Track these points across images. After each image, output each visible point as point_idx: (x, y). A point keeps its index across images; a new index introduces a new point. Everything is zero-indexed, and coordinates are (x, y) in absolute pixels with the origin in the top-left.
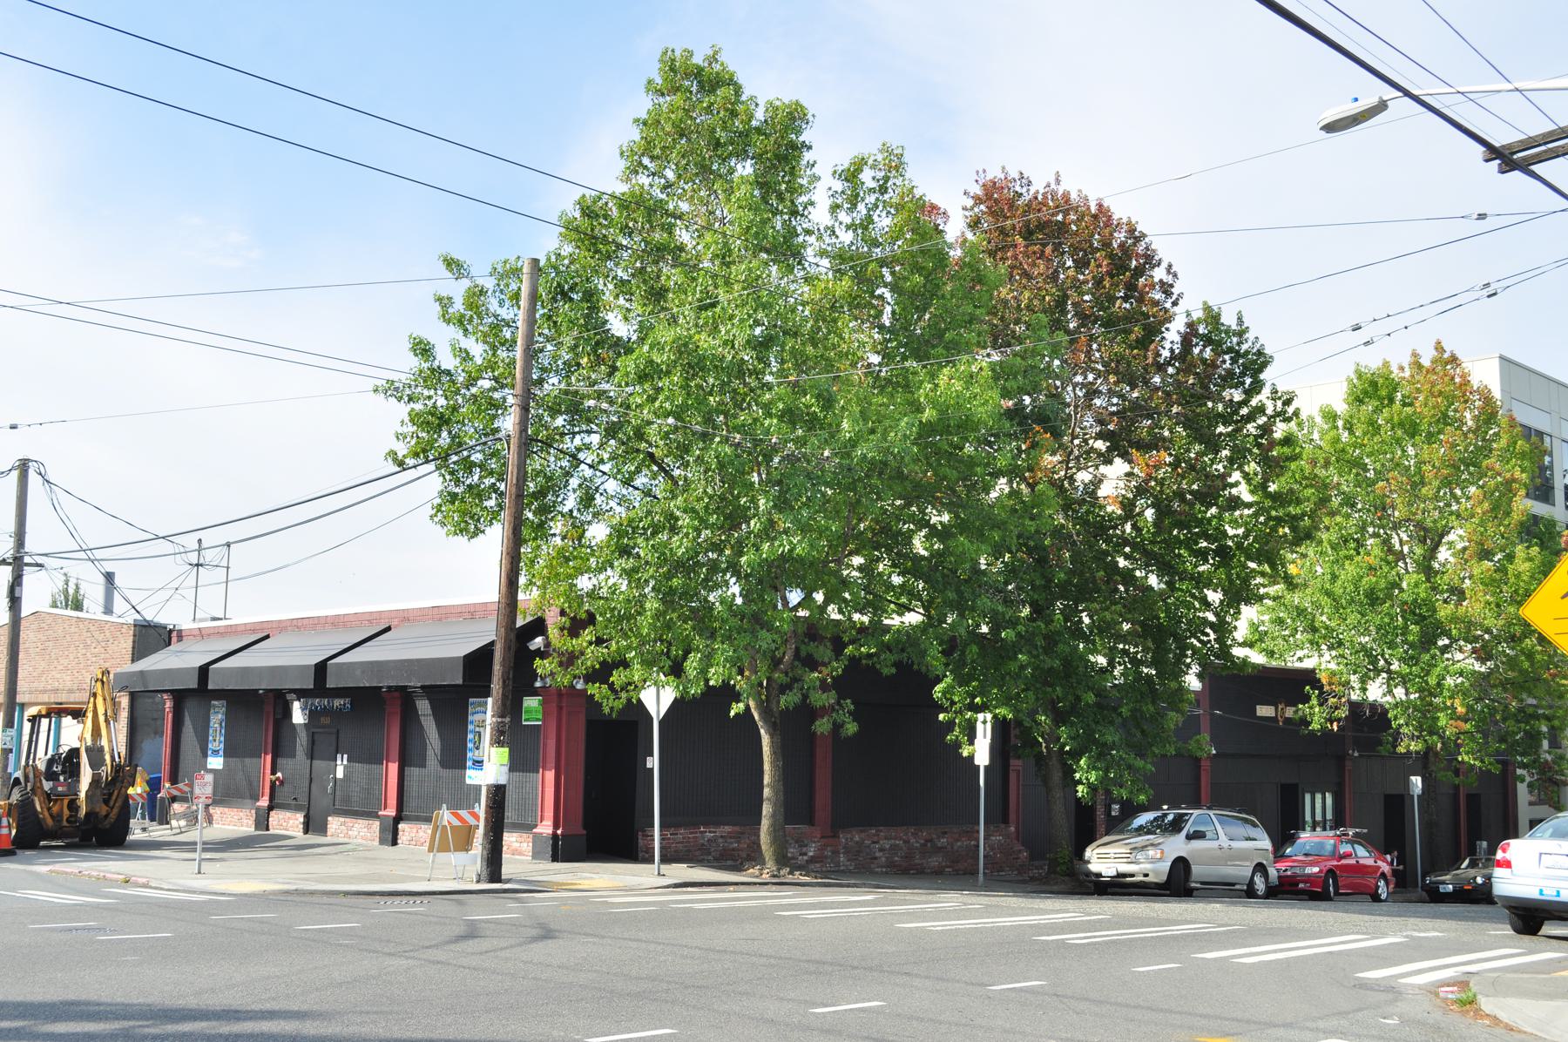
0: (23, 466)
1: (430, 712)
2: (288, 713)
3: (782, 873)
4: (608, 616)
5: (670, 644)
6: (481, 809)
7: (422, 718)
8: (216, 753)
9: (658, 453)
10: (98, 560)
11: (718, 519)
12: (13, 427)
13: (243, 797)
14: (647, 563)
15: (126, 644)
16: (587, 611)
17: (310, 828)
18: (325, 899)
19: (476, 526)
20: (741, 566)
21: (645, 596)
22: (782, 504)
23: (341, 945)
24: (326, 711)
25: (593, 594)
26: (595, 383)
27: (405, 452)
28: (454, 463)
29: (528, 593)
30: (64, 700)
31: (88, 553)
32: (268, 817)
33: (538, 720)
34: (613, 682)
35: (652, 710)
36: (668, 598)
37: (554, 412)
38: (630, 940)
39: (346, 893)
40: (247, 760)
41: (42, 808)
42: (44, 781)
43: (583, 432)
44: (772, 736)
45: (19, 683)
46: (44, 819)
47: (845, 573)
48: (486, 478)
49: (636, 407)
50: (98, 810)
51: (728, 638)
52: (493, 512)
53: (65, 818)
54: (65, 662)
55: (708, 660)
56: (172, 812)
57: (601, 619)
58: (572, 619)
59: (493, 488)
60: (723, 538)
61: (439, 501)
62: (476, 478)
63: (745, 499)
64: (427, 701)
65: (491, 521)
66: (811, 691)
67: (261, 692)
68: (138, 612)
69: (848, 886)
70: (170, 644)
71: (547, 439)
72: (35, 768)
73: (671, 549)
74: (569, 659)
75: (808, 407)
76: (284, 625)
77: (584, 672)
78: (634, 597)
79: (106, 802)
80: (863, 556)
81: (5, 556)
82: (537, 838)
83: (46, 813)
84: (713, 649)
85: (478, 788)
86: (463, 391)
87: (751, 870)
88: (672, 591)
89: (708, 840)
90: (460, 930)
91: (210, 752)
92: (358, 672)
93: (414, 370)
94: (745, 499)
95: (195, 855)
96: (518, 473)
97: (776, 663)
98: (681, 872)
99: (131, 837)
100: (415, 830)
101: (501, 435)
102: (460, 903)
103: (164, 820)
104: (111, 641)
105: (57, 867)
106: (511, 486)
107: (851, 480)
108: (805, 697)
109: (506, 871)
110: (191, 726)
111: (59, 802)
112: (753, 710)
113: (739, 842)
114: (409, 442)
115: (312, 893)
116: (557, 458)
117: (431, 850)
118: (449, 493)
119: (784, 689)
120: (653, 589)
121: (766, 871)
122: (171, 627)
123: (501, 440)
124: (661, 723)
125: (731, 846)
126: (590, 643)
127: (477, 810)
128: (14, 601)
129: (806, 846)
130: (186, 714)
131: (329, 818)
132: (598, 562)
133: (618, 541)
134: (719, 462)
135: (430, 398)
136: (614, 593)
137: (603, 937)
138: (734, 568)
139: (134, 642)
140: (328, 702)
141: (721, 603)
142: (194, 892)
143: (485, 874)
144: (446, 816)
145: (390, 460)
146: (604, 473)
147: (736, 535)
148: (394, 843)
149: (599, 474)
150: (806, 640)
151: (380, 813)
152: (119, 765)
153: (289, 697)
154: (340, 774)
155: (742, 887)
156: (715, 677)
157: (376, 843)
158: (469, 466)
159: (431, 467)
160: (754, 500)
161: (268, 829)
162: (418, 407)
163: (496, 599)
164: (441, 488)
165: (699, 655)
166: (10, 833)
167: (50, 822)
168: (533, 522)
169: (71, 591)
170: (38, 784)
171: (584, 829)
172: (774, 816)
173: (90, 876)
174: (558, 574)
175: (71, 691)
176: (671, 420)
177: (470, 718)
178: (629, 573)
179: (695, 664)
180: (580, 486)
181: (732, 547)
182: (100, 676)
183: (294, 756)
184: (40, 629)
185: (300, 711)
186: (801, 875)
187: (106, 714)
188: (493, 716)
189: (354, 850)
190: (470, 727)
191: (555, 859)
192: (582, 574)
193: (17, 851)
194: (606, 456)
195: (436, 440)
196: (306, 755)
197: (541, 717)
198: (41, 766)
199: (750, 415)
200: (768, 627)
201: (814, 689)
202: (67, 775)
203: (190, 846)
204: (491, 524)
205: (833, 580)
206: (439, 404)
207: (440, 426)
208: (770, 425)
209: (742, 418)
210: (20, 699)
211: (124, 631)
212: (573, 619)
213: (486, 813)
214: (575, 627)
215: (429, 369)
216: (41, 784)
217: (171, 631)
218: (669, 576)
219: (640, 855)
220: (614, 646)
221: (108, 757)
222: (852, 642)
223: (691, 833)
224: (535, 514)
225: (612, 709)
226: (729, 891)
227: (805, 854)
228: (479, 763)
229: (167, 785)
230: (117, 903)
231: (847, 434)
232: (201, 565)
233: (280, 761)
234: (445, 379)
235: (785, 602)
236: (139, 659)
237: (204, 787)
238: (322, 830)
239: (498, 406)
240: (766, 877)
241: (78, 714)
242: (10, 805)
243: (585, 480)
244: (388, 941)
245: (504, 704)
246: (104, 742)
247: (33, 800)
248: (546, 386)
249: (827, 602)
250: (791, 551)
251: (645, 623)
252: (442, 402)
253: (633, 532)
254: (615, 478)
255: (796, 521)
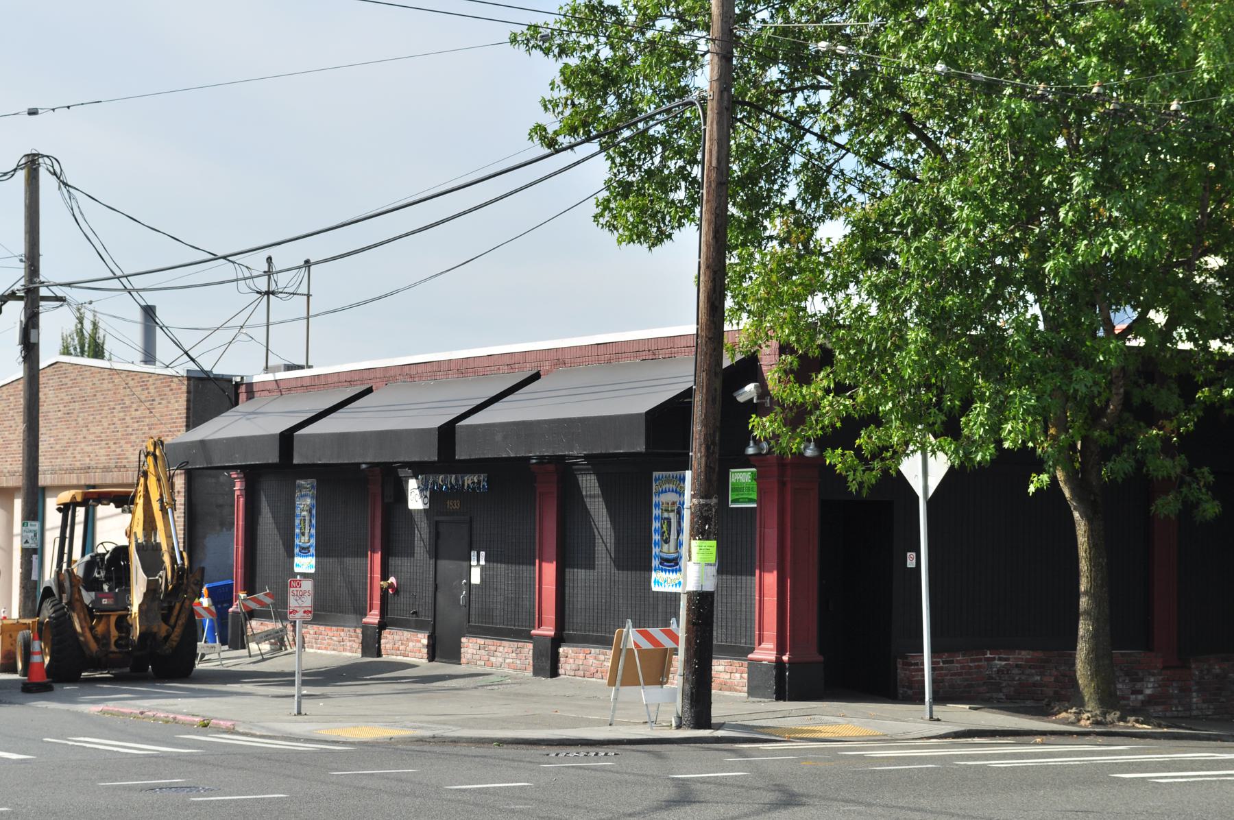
0: (32, 164)
1: (598, 491)
2: (402, 496)
3: (1109, 718)
4: (852, 352)
5: (941, 392)
6: (680, 627)
7: (587, 500)
8: (304, 551)
9: (917, 113)
10: (137, 290)
11: (1011, 207)
12: (33, 112)
13: (346, 612)
14: (907, 274)
15: (178, 404)
16: (820, 346)
17: (438, 652)
18: (474, 750)
19: (659, 228)
20: (1045, 276)
21: (905, 322)
22: (1106, 184)
23: (513, 811)
24: (456, 492)
25: (829, 322)
26: (823, 15)
27: (557, 126)
28: (626, 140)
29: (734, 322)
30: (98, 482)
31: (123, 281)
32: (380, 639)
33: (751, 501)
34: (860, 446)
35: (917, 486)
36: (939, 323)
37: (766, 60)
38: (910, 809)
39: (502, 742)
40: (348, 561)
41: (82, 628)
42: (84, 592)
43: (806, 87)
44: (1090, 521)
45: (41, 459)
46: (86, 643)
47: (1198, 280)
48: (671, 159)
49: (889, 47)
50: (155, 630)
51: (1026, 380)
52: (683, 208)
53: (113, 641)
54: (98, 430)
55: (999, 413)
56: (249, 633)
57: (842, 357)
58: (800, 357)
59: (682, 173)
60: (1017, 235)
61: (606, 194)
62: (657, 160)
63: (1049, 178)
64: (593, 477)
65: (679, 221)
66: (1150, 456)
67: (364, 466)
68: (193, 360)
69: (1209, 738)
70: (237, 404)
71: (758, 100)
72: (70, 572)
73: (944, 254)
74: (798, 416)
75: (1144, 36)
76: (392, 373)
77: (819, 432)
78: (890, 324)
79: (166, 619)
80: (1224, 256)
81: (15, 288)
82: (754, 667)
83: (88, 635)
84: (1007, 397)
85: (675, 597)
86: (636, 36)
87: (1063, 715)
88: (945, 314)
89: (998, 671)
90: (668, 792)
91: (297, 550)
92: (499, 437)
93: (565, 9)
94: (1049, 178)
95: (294, 690)
96: (719, 152)
97: (1095, 415)
98: (960, 715)
99: (199, 666)
100: (582, 656)
101: (694, 96)
102: (659, 756)
103: (238, 641)
104: (158, 400)
105: (111, 706)
106: (709, 170)
107: (1210, 144)
108: (1140, 464)
109: (718, 711)
110: (269, 515)
111: (104, 620)
112: (1062, 484)
113: (1042, 674)
114: (562, 113)
115: (455, 741)
116: (771, 128)
117: (612, 683)
118: (620, 183)
119: (1107, 453)
120: (918, 312)
121: (1085, 716)
122: (238, 379)
123: (693, 104)
124: (930, 503)
125: (1032, 680)
126: (827, 391)
127: (673, 627)
128: (30, 349)
129: (1142, 680)
130: (263, 498)
131: (464, 640)
132: (835, 276)
133: (863, 245)
134: (1012, 124)
135: (590, 47)
136: (859, 318)
137: (870, 805)
138: (1035, 281)
139: (188, 401)
140: (456, 479)
141: (1017, 329)
142: (297, 740)
143: (687, 717)
144: (631, 636)
145: (536, 139)
146: (839, 146)
147: (1037, 231)
148: (554, 673)
149: (831, 147)
150: (1141, 381)
151: (533, 632)
152: (182, 568)
153: (402, 473)
154: (476, 578)
155: (1053, 738)
156: (1012, 434)
157: (529, 673)
158: (646, 143)
159: (594, 146)
160: (1064, 181)
161: (379, 655)
162: (574, 61)
163: (691, 329)
164: (607, 176)
165: (987, 405)
166: (44, 662)
167: (93, 646)
168: (739, 221)
169: (88, 327)
170: (77, 596)
171: (821, 652)
172: (1095, 637)
173: (155, 718)
174: (779, 294)
175: (106, 469)
176: (940, 67)
177: (655, 499)
178: (882, 292)
179: (981, 418)
180: (805, 166)
181: (1031, 249)
182: (151, 449)
183: (412, 554)
184: (61, 386)
185: (417, 491)
186: (1137, 721)
187: (161, 500)
188: (693, 496)
189: (499, 683)
190: (656, 512)
191: (780, 696)
192: (812, 293)
193: (56, 686)
194: (842, 122)
195: (599, 108)
196: (429, 552)
197: (754, 496)
198: (79, 571)
199: (1057, 53)
200: (1089, 363)
201: (1153, 451)
202: (113, 584)
203: (284, 678)
204: (681, 225)
205: (1181, 293)
206: (602, 56)
207: (605, 88)
208: (1088, 67)
209: (1046, 58)
210: (44, 480)
211: (174, 386)
212: (803, 358)
213: (688, 631)
214: (803, 372)
215: (586, 6)
216: (81, 596)
217: (238, 385)
218: (940, 293)
219: (901, 691)
220: (861, 396)
221: (166, 559)
222: (1208, 383)
223: (973, 661)
224: (742, 207)
225: (861, 484)
226: (1036, 744)
227: (1140, 692)
228: (672, 564)
229: (242, 595)
230: (203, 755)
231: (1206, 76)
232: (273, 293)
233: (393, 561)
234: (609, 19)
235: (1110, 326)
236: (196, 425)
237: (301, 599)
238: (454, 655)
239: (688, 56)
240: (1085, 724)
241: (123, 501)
242: (41, 623)
243: (811, 156)
244: (576, 806)
245: (708, 480)
246: (161, 538)
247: (70, 618)
248: (752, 22)
249: (1171, 324)
250: (1120, 251)
251: (907, 360)
252: (606, 53)
253: (886, 231)
254: (857, 153)
255: (1127, 209)
